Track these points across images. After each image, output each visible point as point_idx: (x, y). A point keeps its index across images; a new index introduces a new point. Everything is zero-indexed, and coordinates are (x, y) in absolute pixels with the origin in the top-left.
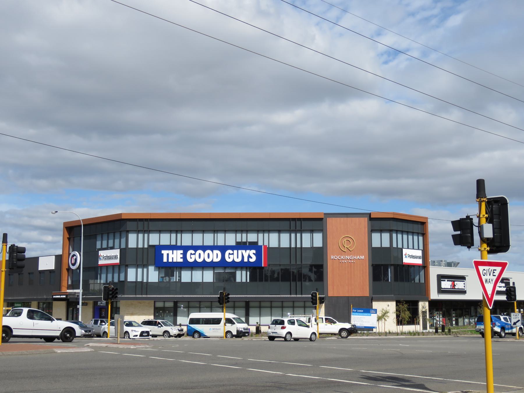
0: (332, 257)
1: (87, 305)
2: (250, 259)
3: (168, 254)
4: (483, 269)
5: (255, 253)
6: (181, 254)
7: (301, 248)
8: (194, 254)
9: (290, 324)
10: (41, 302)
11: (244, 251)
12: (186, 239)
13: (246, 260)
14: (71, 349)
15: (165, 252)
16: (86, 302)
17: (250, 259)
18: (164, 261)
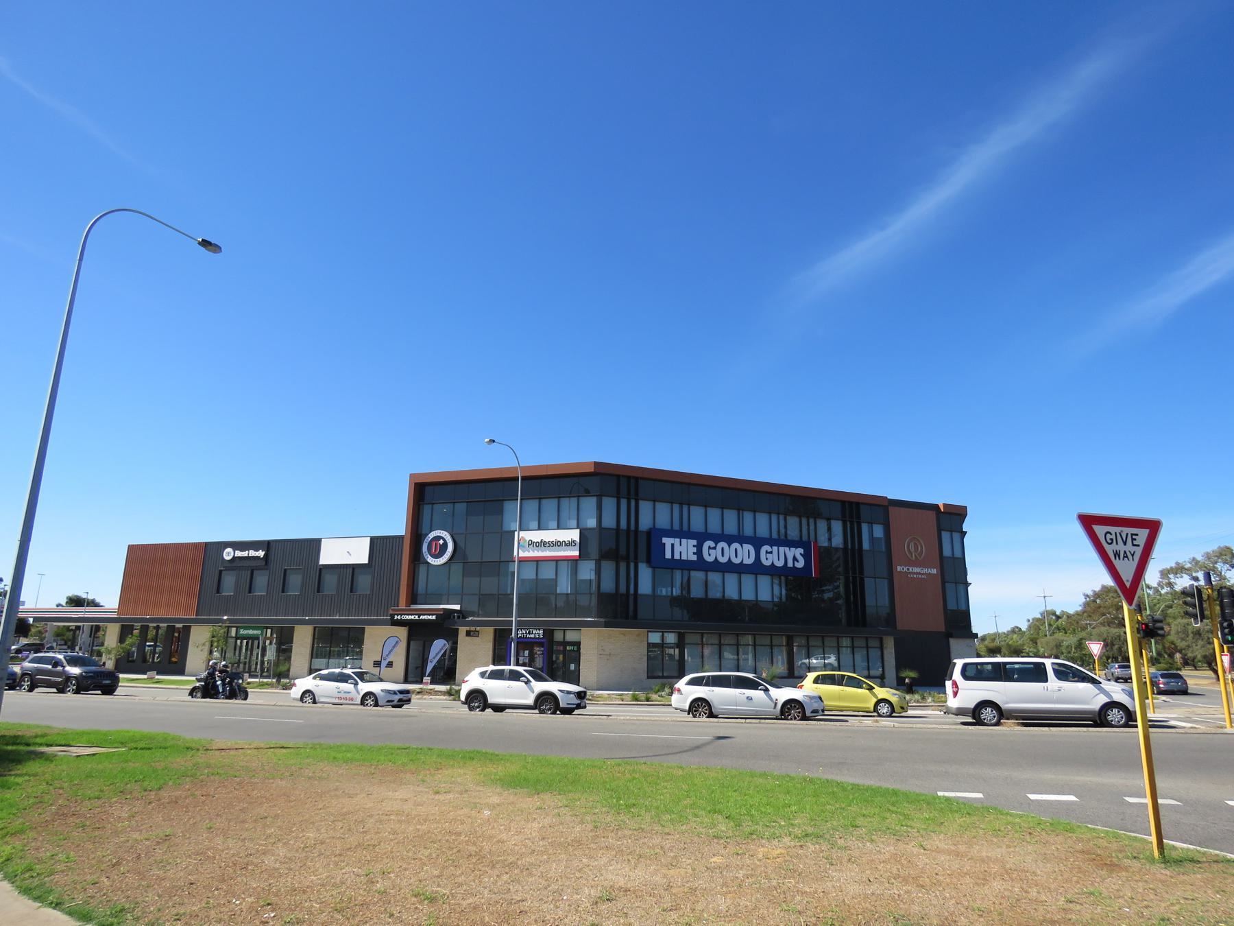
0: (899, 568)
2: (796, 562)
3: (673, 545)
4: (1104, 533)
6: (694, 546)
7: (800, 517)
8: (714, 548)
12: (697, 518)
15: (668, 541)
17: (796, 562)
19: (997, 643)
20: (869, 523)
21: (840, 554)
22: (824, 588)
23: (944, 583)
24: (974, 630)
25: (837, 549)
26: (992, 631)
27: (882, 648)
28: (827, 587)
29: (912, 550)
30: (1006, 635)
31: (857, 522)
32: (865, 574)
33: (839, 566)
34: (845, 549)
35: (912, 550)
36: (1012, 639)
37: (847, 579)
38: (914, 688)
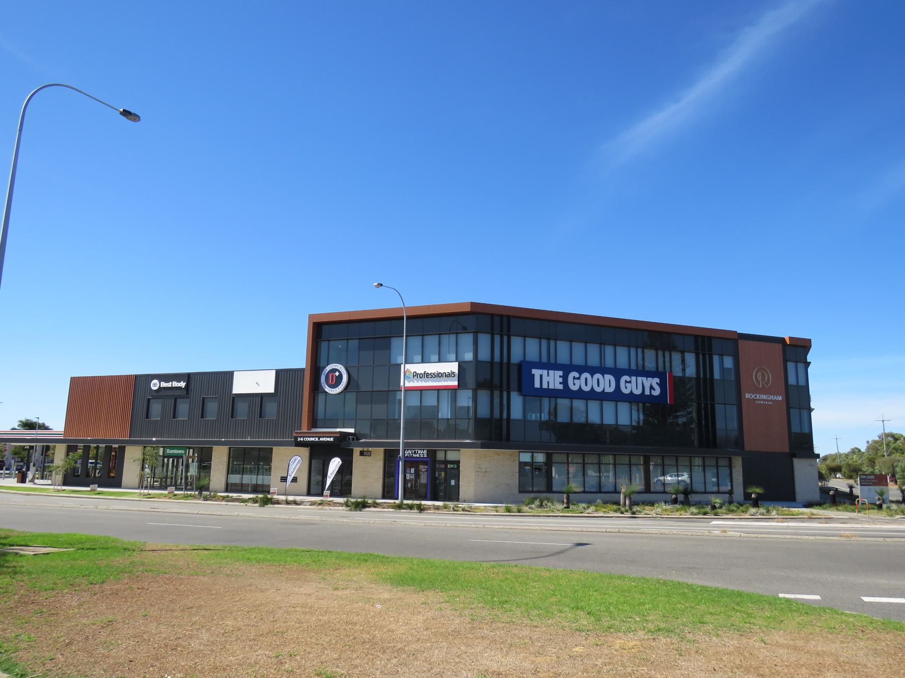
1: (370, 456)
2: (652, 391)
3: (541, 376)
6: (560, 376)
8: (579, 378)
10: (161, 447)
11: (644, 379)
13: (647, 392)
14: (753, 536)
15: (536, 372)
16: (366, 449)
17: (652, 391)
19: (837, 462)
20: (719, 355)
21: (693, 382)
22: (679, 414)
23: (788, 408)
24: (816, 451)
25: (690, 379)
26: (833, 451)
27: (730, 467)
28: (681, 413)
29: (760, 379)
30: (847, 455)
31: (709, 354)
33: (692, 394)
35: (760, 379)
36: (853, 459)
37: (699, 405)
38: (760, 503)
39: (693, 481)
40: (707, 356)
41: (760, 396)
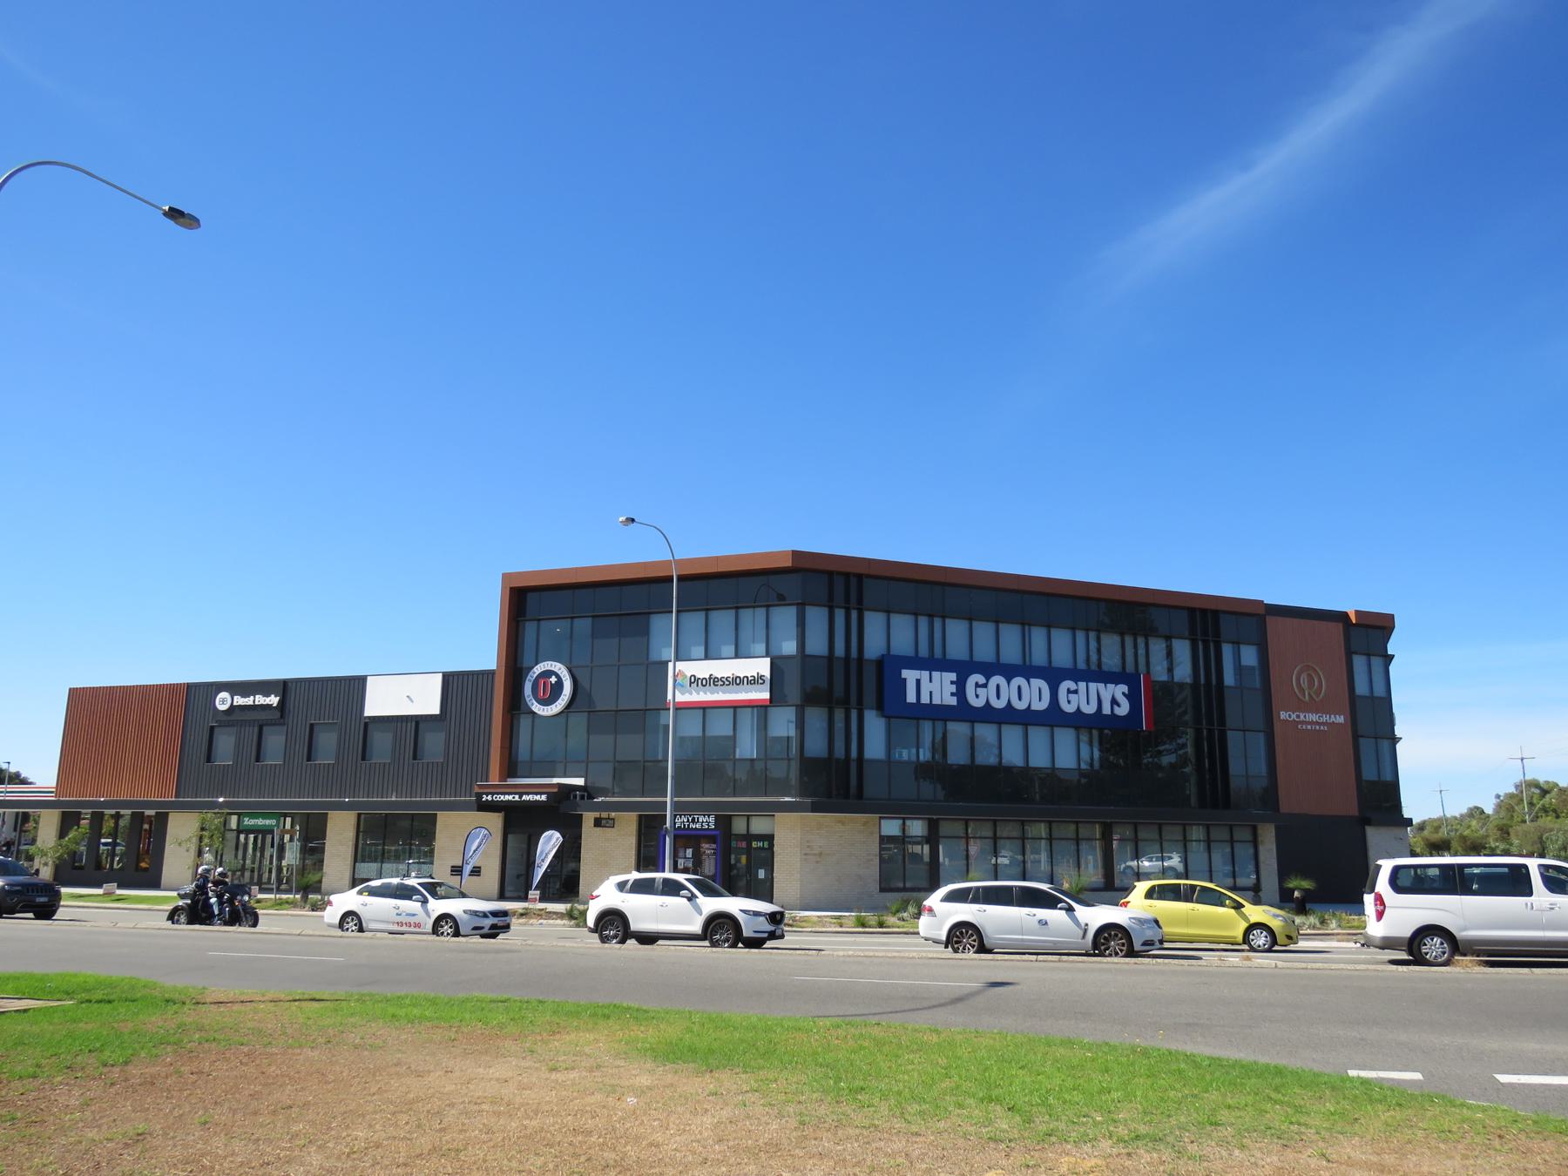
3: (918, 682)
5: (1127, 692)
6: (952, 683)
8: (985, 686)
9: (1126, 893)
12: (956, 639)
15: (910, 675)
18: (908, 701)
19: (1443, 833)
20: (1233, 643)
21: (1187, 692)
22: (1161, 748)
23: (1356, 737)
24: (1406, 814)
25: (1181, 685)
26: (1435, 814)
27: (1255, 843)
28: (1167, 746)
29: (1305, 685)
32: (1229, 723)
33: (1185, 712)
34: (1195, 685)
35: (1305, 685)
37: (1198, 732)
38: (1308, 906)
39: (1189, 868)
40: (1212, 645)
41: (1305, 716)
